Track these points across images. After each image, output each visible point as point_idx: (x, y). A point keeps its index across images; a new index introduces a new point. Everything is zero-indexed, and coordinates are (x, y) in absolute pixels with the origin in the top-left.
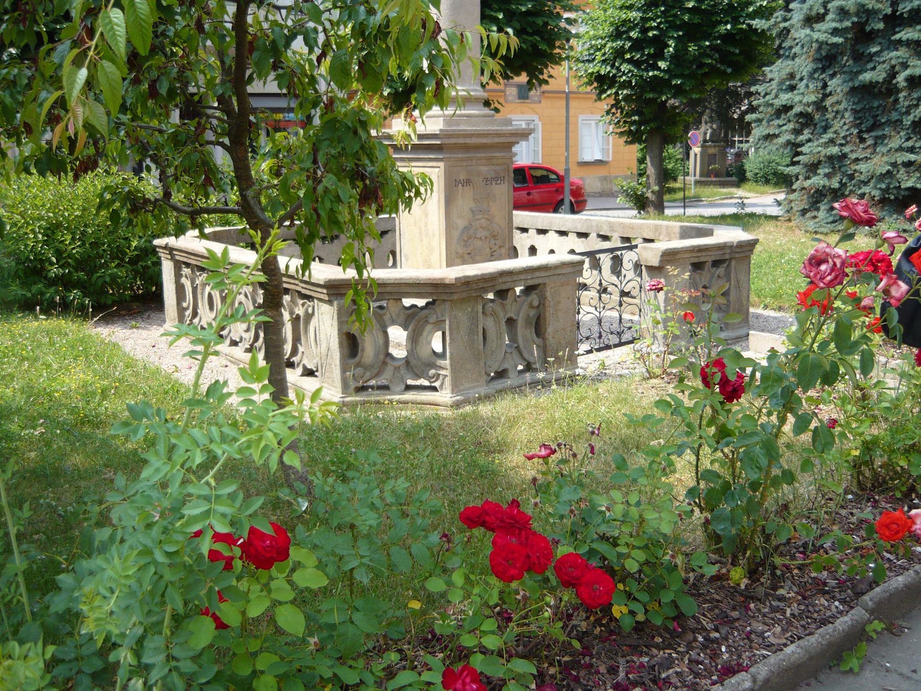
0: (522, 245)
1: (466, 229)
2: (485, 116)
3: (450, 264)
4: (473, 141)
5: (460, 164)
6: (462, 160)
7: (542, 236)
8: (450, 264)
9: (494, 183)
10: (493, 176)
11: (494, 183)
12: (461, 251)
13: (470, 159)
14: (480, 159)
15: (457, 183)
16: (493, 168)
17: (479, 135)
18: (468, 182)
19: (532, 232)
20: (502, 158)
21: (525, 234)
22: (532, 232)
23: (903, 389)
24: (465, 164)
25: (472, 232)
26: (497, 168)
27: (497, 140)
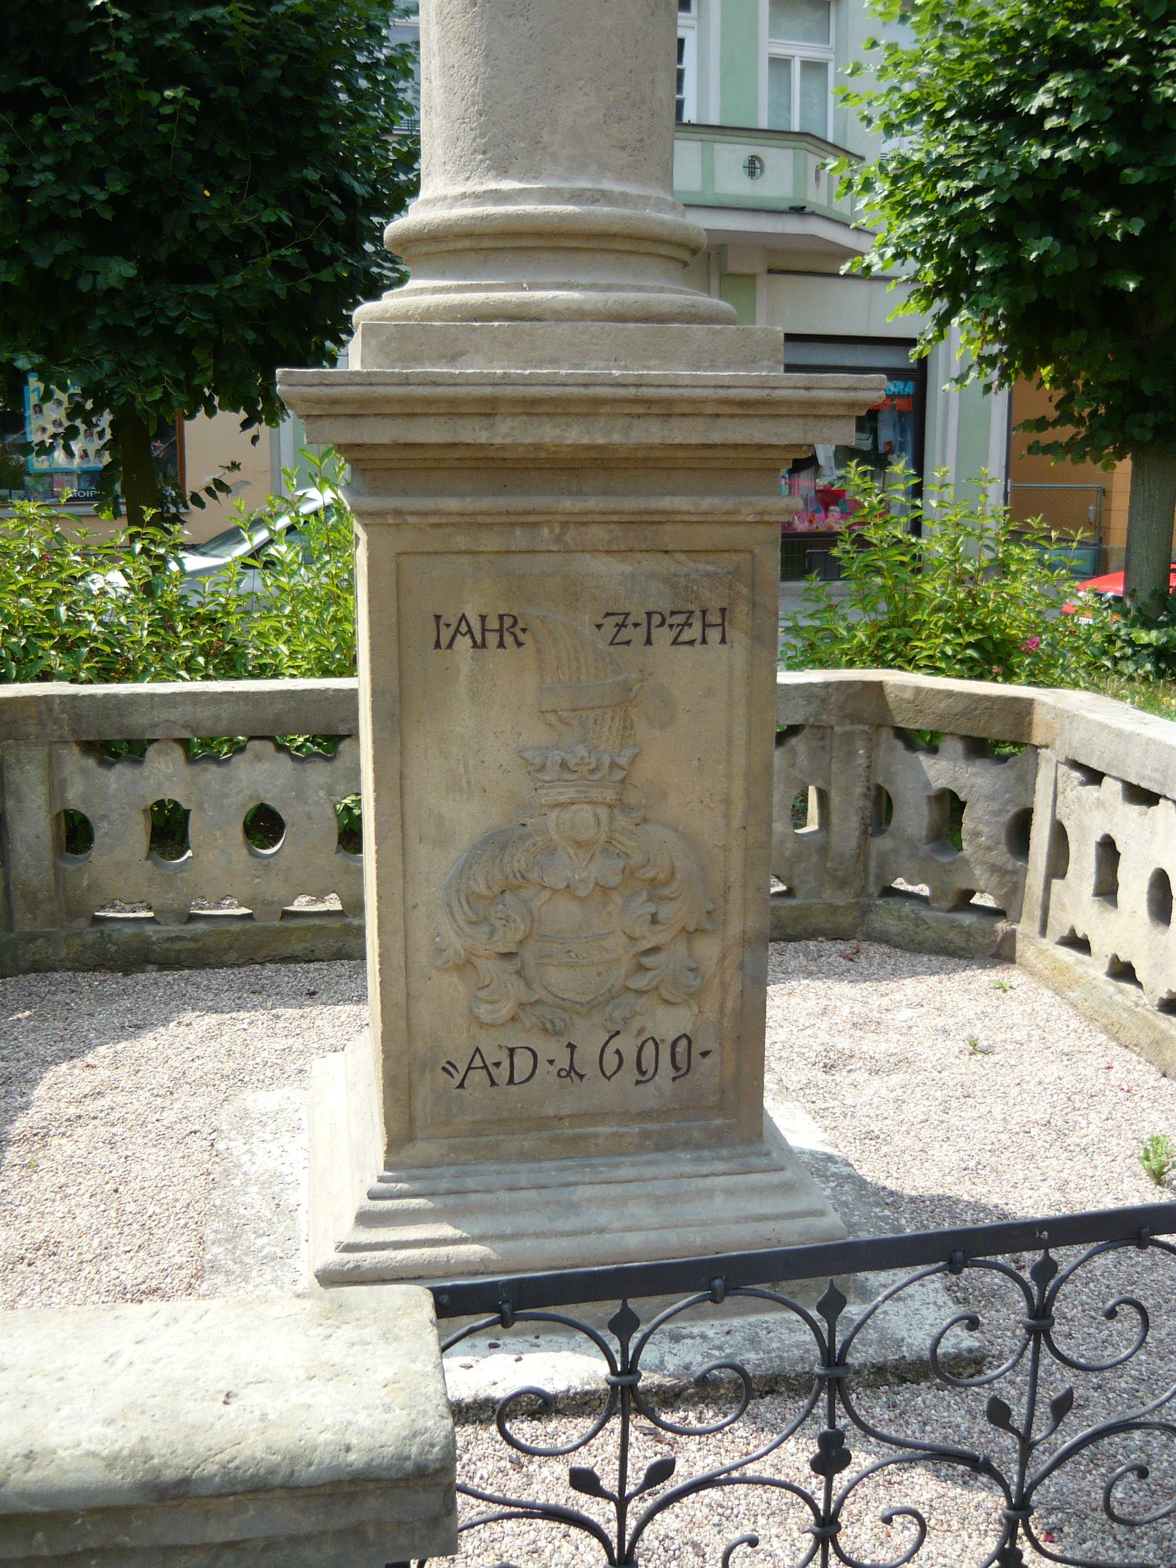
0: (1081, 827)
1: (497, 843)
2: (620, 317)
3: (361, 999)
4: (505, 433)
5: (461, 541)
6: (471, 523)
7: (1136, 809)
8: (361, 999)
9: (663, 636)
10: (665, 606)
11: (663, 636)
12: (456, 944)
13: (527, 521)
14: (582, 521)
15: (445, 632)
16: (664, 565)
17: (589, 407)
18: (508, 630)
19: (1111, 789)
20: (705, 519)
21: (1091, 791)
22: (1111, 789)
23: (1073, 265)
24: (491, 542)
25: (518, 861)
26: (686, 566)
27: (651, 433)
